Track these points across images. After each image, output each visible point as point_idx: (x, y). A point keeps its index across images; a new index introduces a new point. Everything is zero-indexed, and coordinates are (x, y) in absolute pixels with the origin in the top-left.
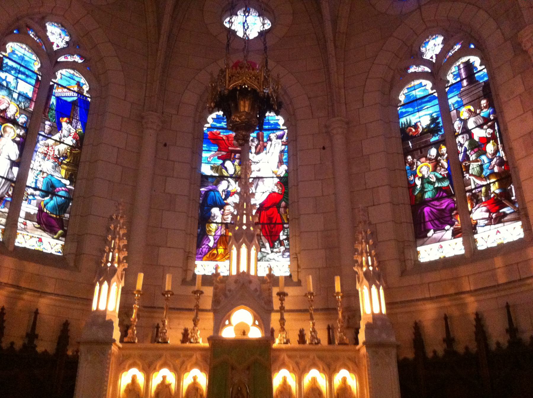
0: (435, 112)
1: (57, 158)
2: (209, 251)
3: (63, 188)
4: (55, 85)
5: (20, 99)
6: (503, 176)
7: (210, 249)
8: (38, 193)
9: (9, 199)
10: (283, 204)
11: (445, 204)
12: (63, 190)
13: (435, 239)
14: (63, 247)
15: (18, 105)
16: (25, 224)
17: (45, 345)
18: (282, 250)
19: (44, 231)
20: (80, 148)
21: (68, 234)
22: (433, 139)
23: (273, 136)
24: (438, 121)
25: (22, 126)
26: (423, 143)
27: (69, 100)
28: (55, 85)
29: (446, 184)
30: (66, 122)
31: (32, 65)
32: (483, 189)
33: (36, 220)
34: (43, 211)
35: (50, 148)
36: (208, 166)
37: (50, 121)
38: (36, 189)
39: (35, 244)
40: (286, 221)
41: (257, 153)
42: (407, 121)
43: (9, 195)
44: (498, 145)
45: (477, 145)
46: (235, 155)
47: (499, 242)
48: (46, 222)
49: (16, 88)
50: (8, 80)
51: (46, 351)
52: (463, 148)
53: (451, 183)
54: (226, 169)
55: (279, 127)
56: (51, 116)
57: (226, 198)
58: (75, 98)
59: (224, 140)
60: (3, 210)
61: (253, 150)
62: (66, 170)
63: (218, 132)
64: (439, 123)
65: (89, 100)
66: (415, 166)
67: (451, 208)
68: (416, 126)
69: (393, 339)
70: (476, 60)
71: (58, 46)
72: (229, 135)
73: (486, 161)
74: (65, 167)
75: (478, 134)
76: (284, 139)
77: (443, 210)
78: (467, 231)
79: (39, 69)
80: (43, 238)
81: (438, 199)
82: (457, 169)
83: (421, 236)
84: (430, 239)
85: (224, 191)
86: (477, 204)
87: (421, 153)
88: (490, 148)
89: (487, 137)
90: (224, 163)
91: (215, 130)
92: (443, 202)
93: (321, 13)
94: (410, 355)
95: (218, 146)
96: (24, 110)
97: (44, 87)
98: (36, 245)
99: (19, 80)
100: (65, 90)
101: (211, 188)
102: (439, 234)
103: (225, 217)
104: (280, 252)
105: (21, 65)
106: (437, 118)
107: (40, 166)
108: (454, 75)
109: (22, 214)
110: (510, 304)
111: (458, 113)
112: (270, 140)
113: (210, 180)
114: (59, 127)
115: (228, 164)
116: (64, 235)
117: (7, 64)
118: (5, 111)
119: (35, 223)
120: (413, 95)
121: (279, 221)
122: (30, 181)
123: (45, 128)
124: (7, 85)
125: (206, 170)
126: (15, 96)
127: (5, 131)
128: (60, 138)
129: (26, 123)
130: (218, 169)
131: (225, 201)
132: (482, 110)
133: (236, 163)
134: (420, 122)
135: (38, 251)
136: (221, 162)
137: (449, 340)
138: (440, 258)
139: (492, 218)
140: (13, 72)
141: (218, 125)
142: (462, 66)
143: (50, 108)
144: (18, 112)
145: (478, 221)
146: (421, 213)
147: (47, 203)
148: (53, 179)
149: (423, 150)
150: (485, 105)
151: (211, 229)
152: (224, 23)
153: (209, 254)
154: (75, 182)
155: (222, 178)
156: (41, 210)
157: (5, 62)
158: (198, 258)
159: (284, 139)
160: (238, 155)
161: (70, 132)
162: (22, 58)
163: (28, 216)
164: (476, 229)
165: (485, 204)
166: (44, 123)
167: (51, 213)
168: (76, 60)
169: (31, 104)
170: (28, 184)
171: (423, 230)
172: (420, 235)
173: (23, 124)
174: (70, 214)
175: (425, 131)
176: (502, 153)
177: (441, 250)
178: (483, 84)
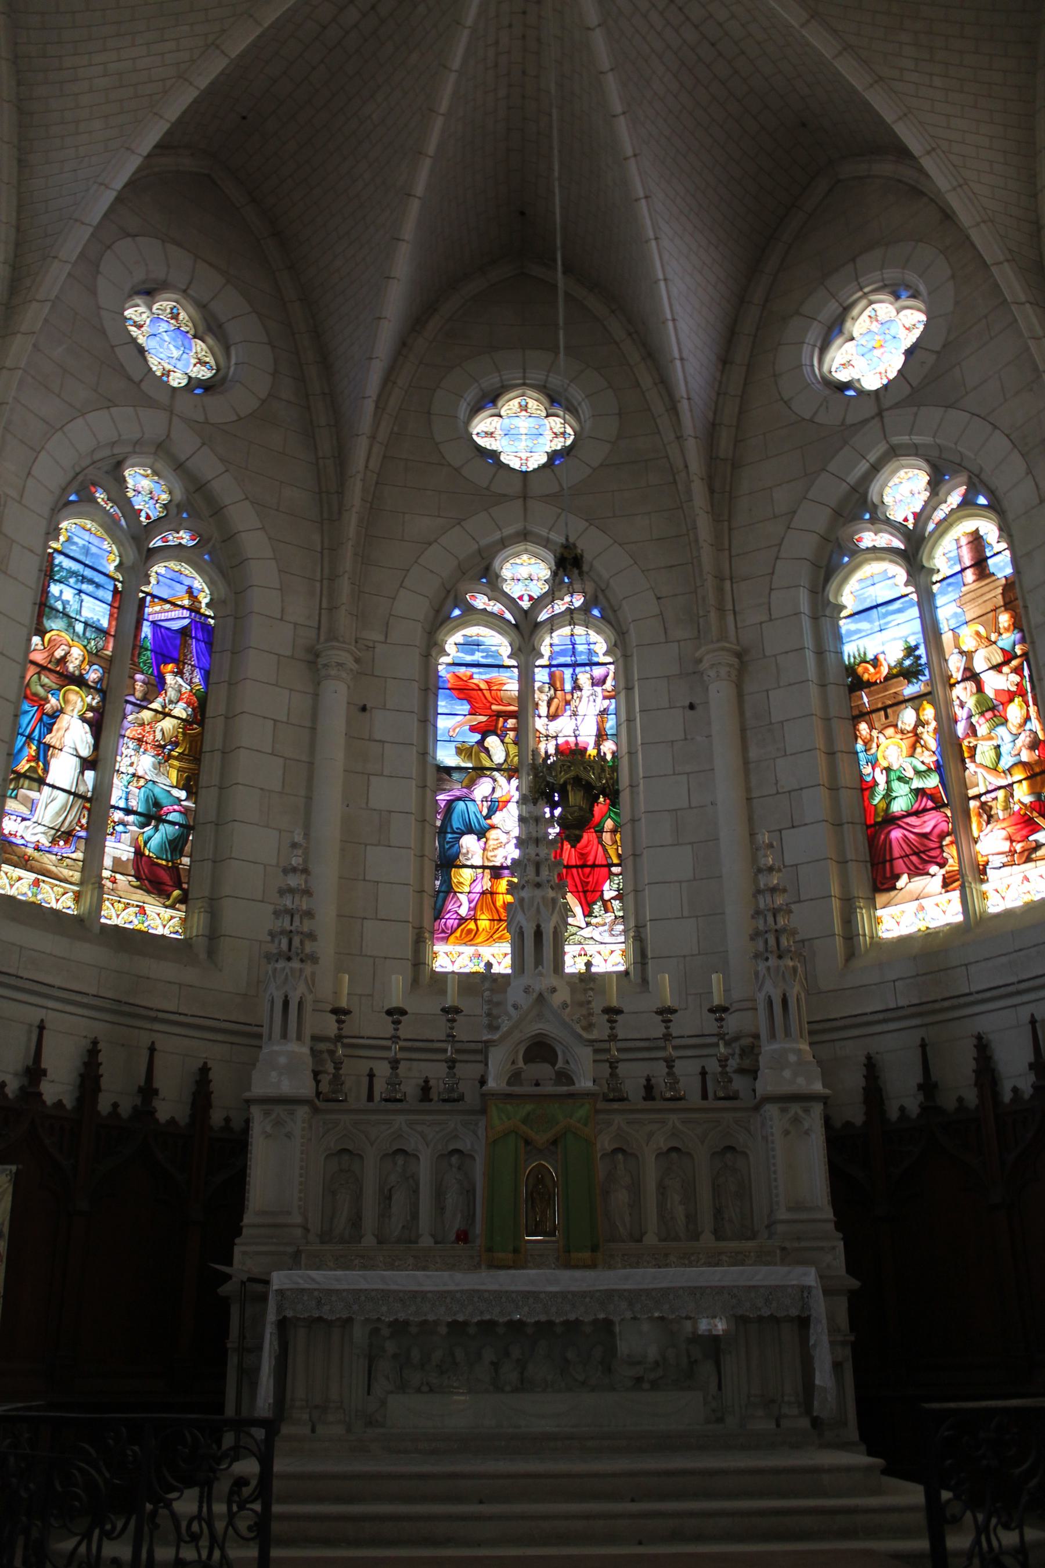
0: (914, 634)
1: (160, 746)
2: (459, 925)
3: (176, 807)
4: (149, 598)
5: (88, 634)
6: (1037, 770)
7: (462, 920)
8: (131, 818)
9: (83, 834)
10: (609, 824)
11: (929, 823)
12: (175, 811)
13: (911, 892)
14: (184, 921)
15: (85, 647)
16: (114, 882)
17: (171, 1105)
18: (608, 920)
19: (148, 892)
20: (201, 723)
21: (190, 896)
22: (910, 690)
23: (584, 679)
24: (917, 653)
25: (95, 688)
26: (888, 697)
27: (176, 625)
28: (149, 598)
29: (932, 782)
30: (173, 672)
31: (104, 562)
32: (1001, 794)
33: (133, 873)
34: (143, 854)
35: (147, 728)
36: (451, 749)
37: (143, 673)
38: (128, 811)
39: (132, 918)
40: (616, 861)
41: (552, 717)
42: (858, 650)
43: (82, 827)
44: (1028, 706)
45: (991, 705)
46: (505, 721)
47: (1027, 898)
48: (153, 877)
49: (80, 612)
50: (64, 597)
51: (173, 1118)
52: (966, 710)
53: (942, 781)
54: (487, 751)
55: (595, 659)
56: (145, 663)
57: (488, 817)
58: (186, 622)
59: (481, 690)
60: (74, 856)
61: (543, 710)
62: (178, 771)
63: (469, 674)
64: (919, 657)
65: (212, 622)
66: (874, 745)
67: (943, 831)
68: (875, 662)
69: (818, 1087)
70: (989, 530)
71: (148, 517)
72: (491, 679)
73: (1008, 738)
74: (176, 763)
75: (995, 683)
76: (609, 684)
77: (925, 836)
78: (968, 877)
79: (118, 568)
80: (147, 907)
81: (917, 813)
82: (954, 755)
83: (885, 886)
84: (901, 894)
85: (485, 799)
86: (988, 823)
87: (887, 717)
88: (1015, 711)
89: (1009, 691)
90: (483, 739)
91: (463, 669)
92: (926, 818)
93: (677, 414)
94: (857, 1115)
95: (469, 702)
96: (96, 655)
97: (128, 603)
98: (136, 922)
99: (83, 596)
100: (167, 606)
101: (458, 793)
102: (919, 883)
103: (490, 854)
104: (604, 925)
105: (86, 565)
106: (916, 647)
107: (132, 764)
108: (949, 559)
109: (108, 862)
110: (1038, 1017)
111: (956, 637)
112: (577, 687)
113: (456, 776)
114: (160, 684)
115: (492, 742)
116: (184, 900)
117: (60, 565)
118: (63, 660)
119: (130, 878)
120: (870, 596)
121: (601, 860)
122: (117, 797)
123: (134, 689)
124: (64, 608)
125: (447, 756)
126: (79, 628)
127: (66, 701)
128: (164, 707)
129: (101, 680)
130: (471, 754)
131: (489, 821)
132: (1000, 634)
133: (507, 740)
134: (883, 653)
135: (140, 931)
136: (477, 737)
137: (928, 1087)
138: (919, 930)
139: (1015, 852)
140: (72, 581)
141: (468, 659)
142: (964, 541)
143: (141, 647)
144: (86, 662)
145: (991, 858)
146: (885, 839)
147: (150, 838)
148: (157, 791)
149: (889, 711)
150: (1006, 625)
151: (462, 880)
152: (475, 437)
153: (460, 930)
154: (196, 794)
155: (480, 771)
156: (139, 853)
157: (57, 562)
158: (438, 939)
159: (609, 684)
160: (511, 723)
161: (180, 691)
162: (87, 551)
163: (118, 866)
164: (985, 874)
165: (1004, 825)
166: (132, 678)
167: (157, 858)
168: (184, 542)
169: (107, 641)
170: (113, 802)
171: (888, 875)
172: (883, 882)
173: (97, 683)
174: (190, 856)
175: (895, 671)
176: (1035, 725)
177: (921, 915)
178: (1003, 581)
